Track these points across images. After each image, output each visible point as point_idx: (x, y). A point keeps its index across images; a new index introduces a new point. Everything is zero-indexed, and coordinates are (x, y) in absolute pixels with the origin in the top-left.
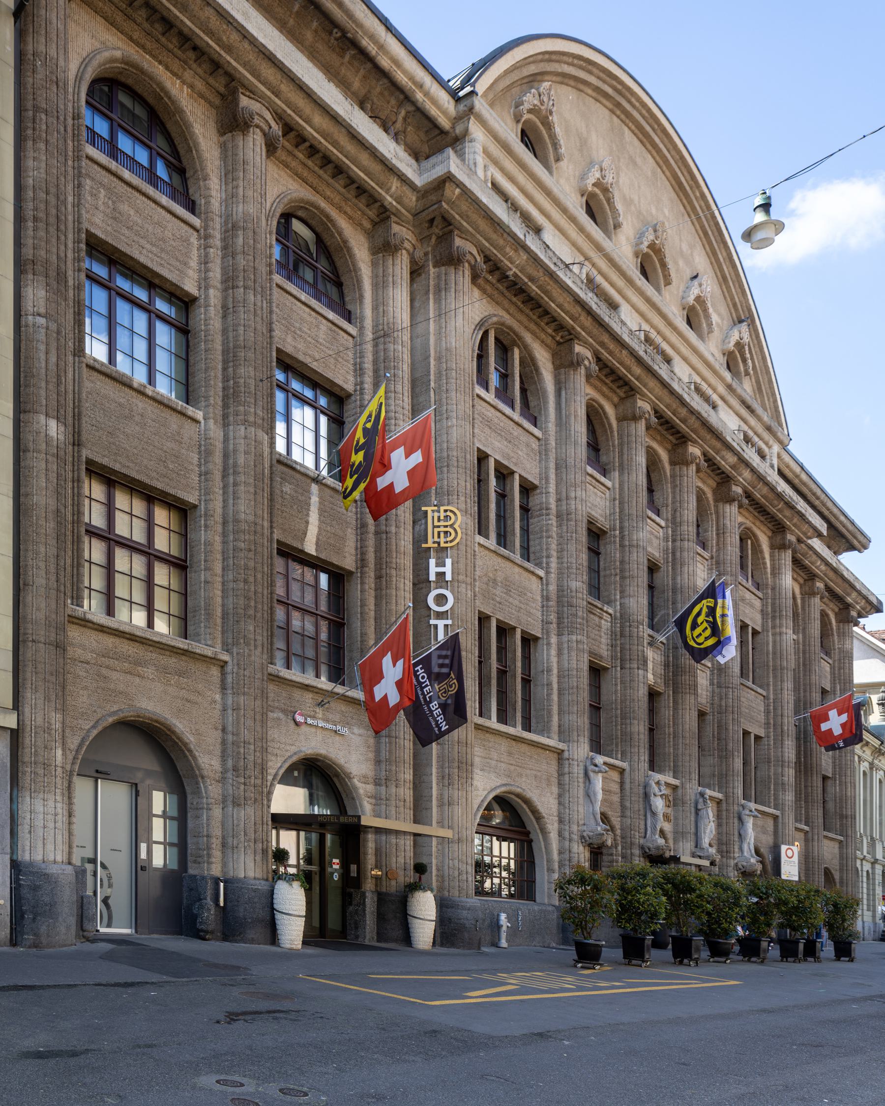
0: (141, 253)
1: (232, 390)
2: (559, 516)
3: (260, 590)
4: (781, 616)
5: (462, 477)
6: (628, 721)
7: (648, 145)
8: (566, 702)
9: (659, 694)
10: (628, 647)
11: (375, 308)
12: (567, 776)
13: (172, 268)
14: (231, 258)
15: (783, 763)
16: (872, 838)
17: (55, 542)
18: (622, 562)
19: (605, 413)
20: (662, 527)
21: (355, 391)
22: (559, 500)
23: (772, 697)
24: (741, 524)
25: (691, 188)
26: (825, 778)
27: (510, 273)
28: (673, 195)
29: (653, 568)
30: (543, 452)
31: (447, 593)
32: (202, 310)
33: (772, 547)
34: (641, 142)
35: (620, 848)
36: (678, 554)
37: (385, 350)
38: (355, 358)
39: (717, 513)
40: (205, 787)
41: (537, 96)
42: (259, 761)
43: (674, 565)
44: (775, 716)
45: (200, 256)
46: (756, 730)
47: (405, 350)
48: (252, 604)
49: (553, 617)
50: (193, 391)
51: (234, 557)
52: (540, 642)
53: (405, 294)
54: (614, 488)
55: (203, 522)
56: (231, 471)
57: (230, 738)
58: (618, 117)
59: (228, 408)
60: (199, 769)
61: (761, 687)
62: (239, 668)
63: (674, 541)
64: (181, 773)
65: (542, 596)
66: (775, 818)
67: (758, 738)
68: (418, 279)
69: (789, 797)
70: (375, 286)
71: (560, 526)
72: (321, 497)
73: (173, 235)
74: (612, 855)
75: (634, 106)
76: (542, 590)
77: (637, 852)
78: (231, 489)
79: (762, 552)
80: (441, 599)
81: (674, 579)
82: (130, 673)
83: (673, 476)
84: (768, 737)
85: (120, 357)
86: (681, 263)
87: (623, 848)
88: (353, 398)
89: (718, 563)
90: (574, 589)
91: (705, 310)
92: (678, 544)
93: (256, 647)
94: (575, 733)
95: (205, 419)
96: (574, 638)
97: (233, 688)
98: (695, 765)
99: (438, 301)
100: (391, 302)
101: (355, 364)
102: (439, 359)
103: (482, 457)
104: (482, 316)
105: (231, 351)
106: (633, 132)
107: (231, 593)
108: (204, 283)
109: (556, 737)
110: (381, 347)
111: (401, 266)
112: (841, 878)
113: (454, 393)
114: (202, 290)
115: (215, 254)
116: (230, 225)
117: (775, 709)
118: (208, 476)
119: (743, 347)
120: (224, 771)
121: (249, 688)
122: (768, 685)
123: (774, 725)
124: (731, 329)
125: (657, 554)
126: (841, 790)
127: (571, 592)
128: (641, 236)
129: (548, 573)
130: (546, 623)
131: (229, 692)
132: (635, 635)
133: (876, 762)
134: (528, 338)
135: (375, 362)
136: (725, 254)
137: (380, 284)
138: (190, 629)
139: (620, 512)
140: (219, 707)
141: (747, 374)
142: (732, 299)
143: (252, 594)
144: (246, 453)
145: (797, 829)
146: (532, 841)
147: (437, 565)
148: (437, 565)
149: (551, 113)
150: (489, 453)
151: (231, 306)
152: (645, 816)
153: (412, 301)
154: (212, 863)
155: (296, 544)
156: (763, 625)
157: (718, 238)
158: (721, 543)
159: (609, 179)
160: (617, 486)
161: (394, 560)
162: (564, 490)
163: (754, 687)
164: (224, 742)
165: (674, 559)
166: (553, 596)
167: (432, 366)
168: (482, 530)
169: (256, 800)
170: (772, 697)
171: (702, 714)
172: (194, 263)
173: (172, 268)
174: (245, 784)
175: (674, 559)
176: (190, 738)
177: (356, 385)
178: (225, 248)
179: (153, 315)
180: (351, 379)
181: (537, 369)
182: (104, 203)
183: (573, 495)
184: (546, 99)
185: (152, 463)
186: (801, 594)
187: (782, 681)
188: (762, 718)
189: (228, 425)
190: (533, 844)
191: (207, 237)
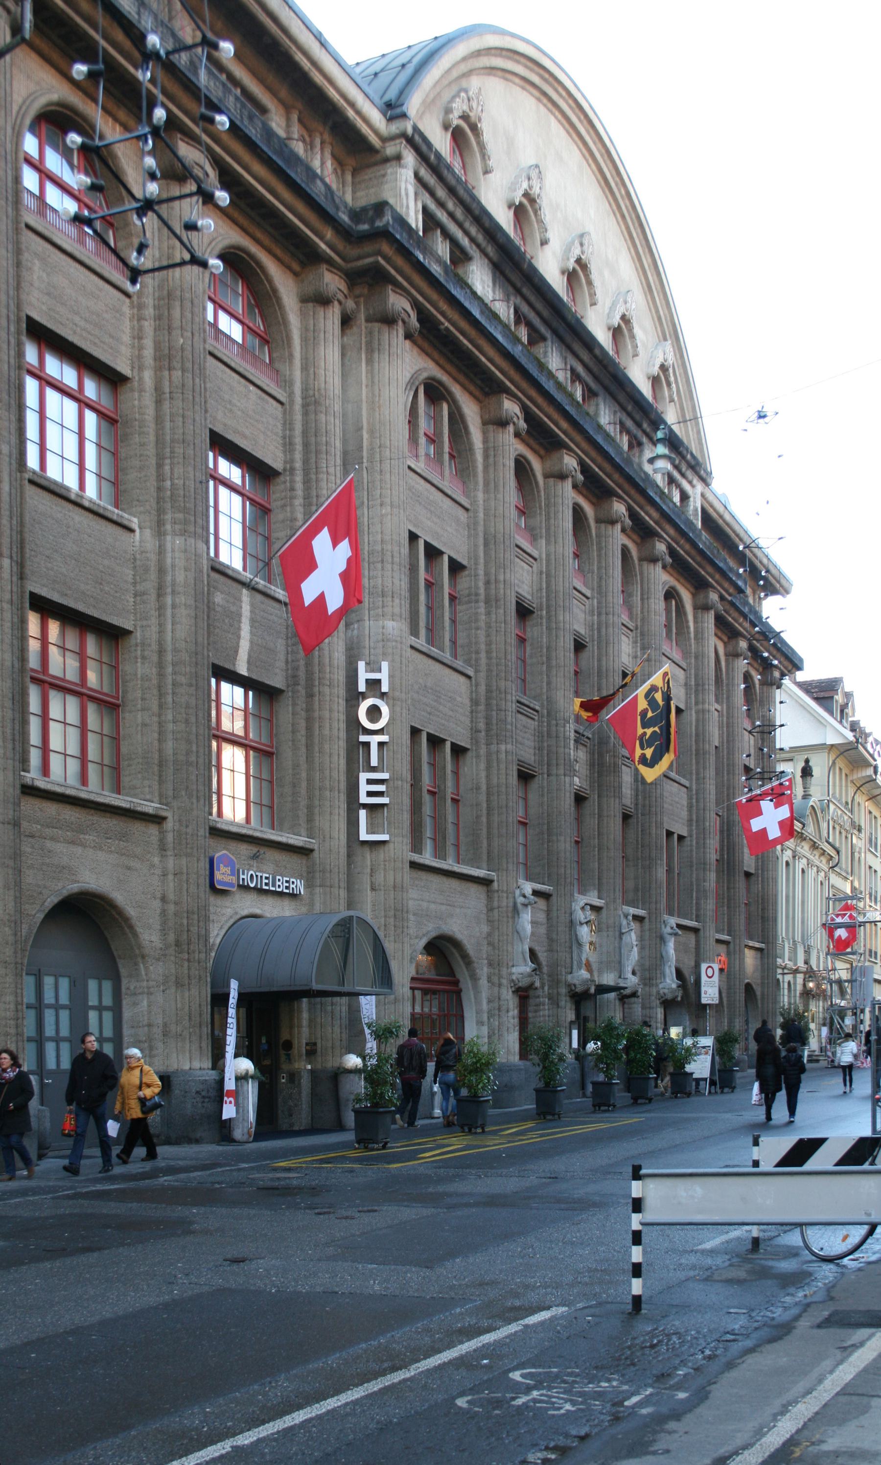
0: (75, 333)
1: (169, 493)
2: (487, 601)
3: (201, 732)
4: (704, 690)
5: (396, 575)
6: (555, 838)
7: (574, 136)
8: (496, 825)
9: (585, 799)
10: (554, 749)
11: (305, 368)
12: (496, 911)
13: (106, 347)
14: (166, 332)
15: (703, 865)
16: (794, 941)
17: (10, 702)
18: (548, 648)
19: (532, 470)
20: (587, 598)
21: (285, 470)
22: (487, 583)
23: (694, 787)
24: (664, 583)
25: (617, 185)
26: (748, 875)
27: (442, 327)
28: (599, 191)
29: (579, 646)
30: (472, 526)
31: (385, 710)
32: (136, 395)
33: (696, 608)
34: (568, 132)
35: (546, 988)
36: (604, 630)
37: (316, 421)
38: (284, 430)
39: (641, 574)
40: (146, 969)
41: (466, 101)
42: (203, 932)
43: (599, 643)
44: (698, 809)
45: (133, 328)
46: (680, 829)
47: (337, 421)
48: (194, 748)
49: (482, 726)
50: (125, 491)
51: (173, 693)
52: (469, 754)
53: (336, 349)
54: (541, 559)
55: (139, 652)
56: (169, 590)
57: (171, 908)
58: (545, 105)
59: (165, 513)
60: (140, 947)
61: (684, 777)
62: (181, 825)
63: (599, 614)
64: (115, 953)
65: (471, 700)
66: (696, 930)
67: (681, 838)
68: (348, 332)
69: (710, 905)
70: (304, 340)
71: (488, 614)
72: (252, 605)
73: (106, 305)
74: (538, 997)
75: (561, 95)
76: (472, 692)
77: (563, 990)
78: (169, 612)
79: (685, 614)
80: (374, 713)
81: (599, 660)
82: (73, 843)
83: (598, 536)
84: (691, 836)
85: (51, 459)
86: (606, 273)
87: (550, 987)
88: (282, 478)
89: (642, 634)
90: (503, 689)
91: (630, 330)
92: (603, 617)
93: (198, 798)
94: (504, 860)
95: (140, 528)
96: (503, 747)
97: (174, 848)
98: (619, 881)
99: (370, 361)
100: (322, 364)
101: (284, 437)
102: (371, 432)
103: (413, 537)
104: (413, 372)
105: (168, 445)
106: (559, 121)
107: (170, 736)
108: (138, 362)
109: (485, 865)
110: (312, 416)
111: (331, 318)
112: (763, 994)
113: (388, 476)
114: (136, 370)
115: (148, 326)
116: (165, 292)
117: (697, 801)
118: (145, 597)
119: (667, 370)
120: (167, 947)
121: (192, 848)
122: (691, 774)
123: (697, 821)
124: (656, 348)
125: (582, 632)
126: (763, 888)
127: (500, 693)
128: (568, 249)
129: (477, 671)
130: (475, 731)
131: (169, 853)
132: (562, 735)
133: (798, 848)
134: (457, 391)
135: (305, 433)
136: (650, 260)
137: (310, 339)
138: (125, 780)
139: (547, 588)
140: (158, 872)
141: (672, 400)
142: (657, 311)
143: (193, 737)
144: (186, 569)
145: (718, 941)
146: (461, 990)
147: (379, 682)
148: (379, 682)
149: (480, 120)
150: (419, 534)
151: (167, 390)
152: (571, 947)
153: (343, 355)
154: (154, 1056)
155: (227, 666)
156: (687, 703)
157: (644, 242)
158: (645, 610)
159: (536, 191)
160: (544, 556)
161: (328, 676)
162: (493, 571)
163: (677, 778)
164: (164, 913)
165: (599, 636)
166: (483, 700)
167: (365, 441)
168: (415, 632)
169: (200, 977)
170: (694, 787)
171: (626, 817)
172: (126, 338)
173: (106, 347)
174: (189, 960)
175: (599, 636)
176: (131, 912)
177: (285, 462)
178: (158, 318)
179: (83, 403)
180: (280, 455)
181: (466, 428)
182: (38, 278)
183: (501, 578)
184: (474, 105)
185: (89, 587)
186: (726, 655)
187: (704, 768)
188: (684, 814)
189: (165, 534)
190: (463, 994)
191: (141, 307)
